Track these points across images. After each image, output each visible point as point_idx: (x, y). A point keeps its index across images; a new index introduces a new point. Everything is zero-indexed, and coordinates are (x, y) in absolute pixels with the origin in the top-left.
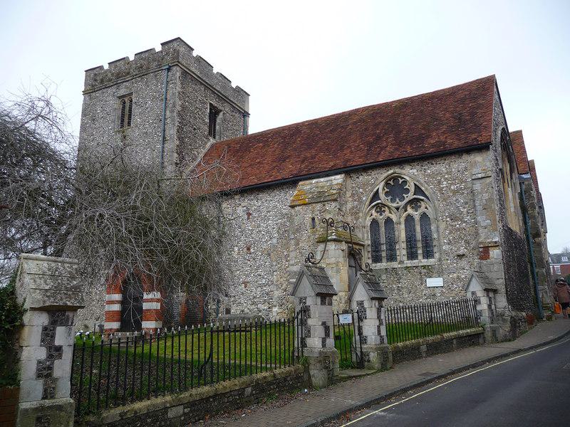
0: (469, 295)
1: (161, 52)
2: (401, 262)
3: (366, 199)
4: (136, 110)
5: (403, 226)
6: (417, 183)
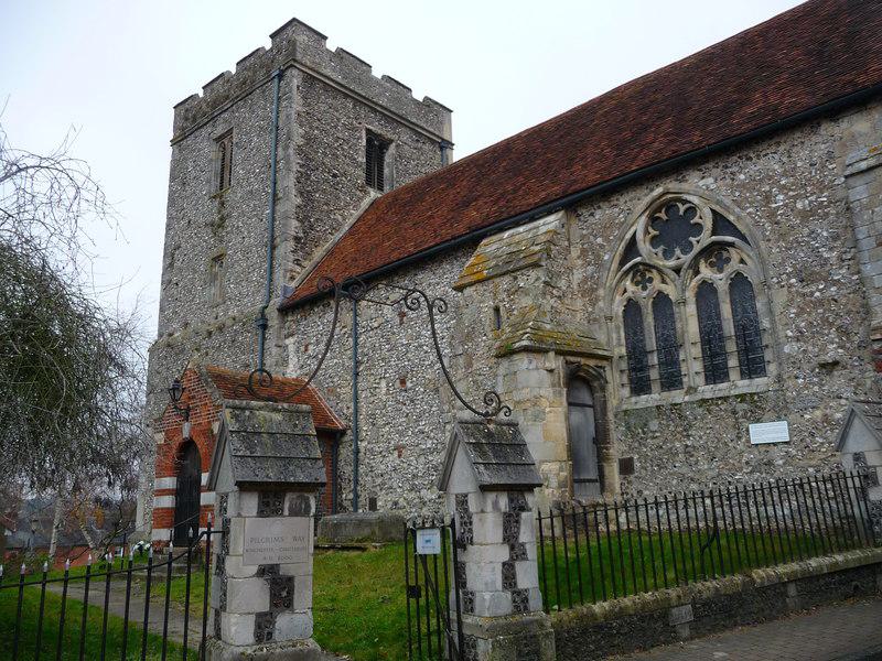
0: (848, 464)
1: (271, 50)
2: (692, 390)
3: (611, 257)
4: (238, 156)
5: (691, 309)
6: (717, 208)
